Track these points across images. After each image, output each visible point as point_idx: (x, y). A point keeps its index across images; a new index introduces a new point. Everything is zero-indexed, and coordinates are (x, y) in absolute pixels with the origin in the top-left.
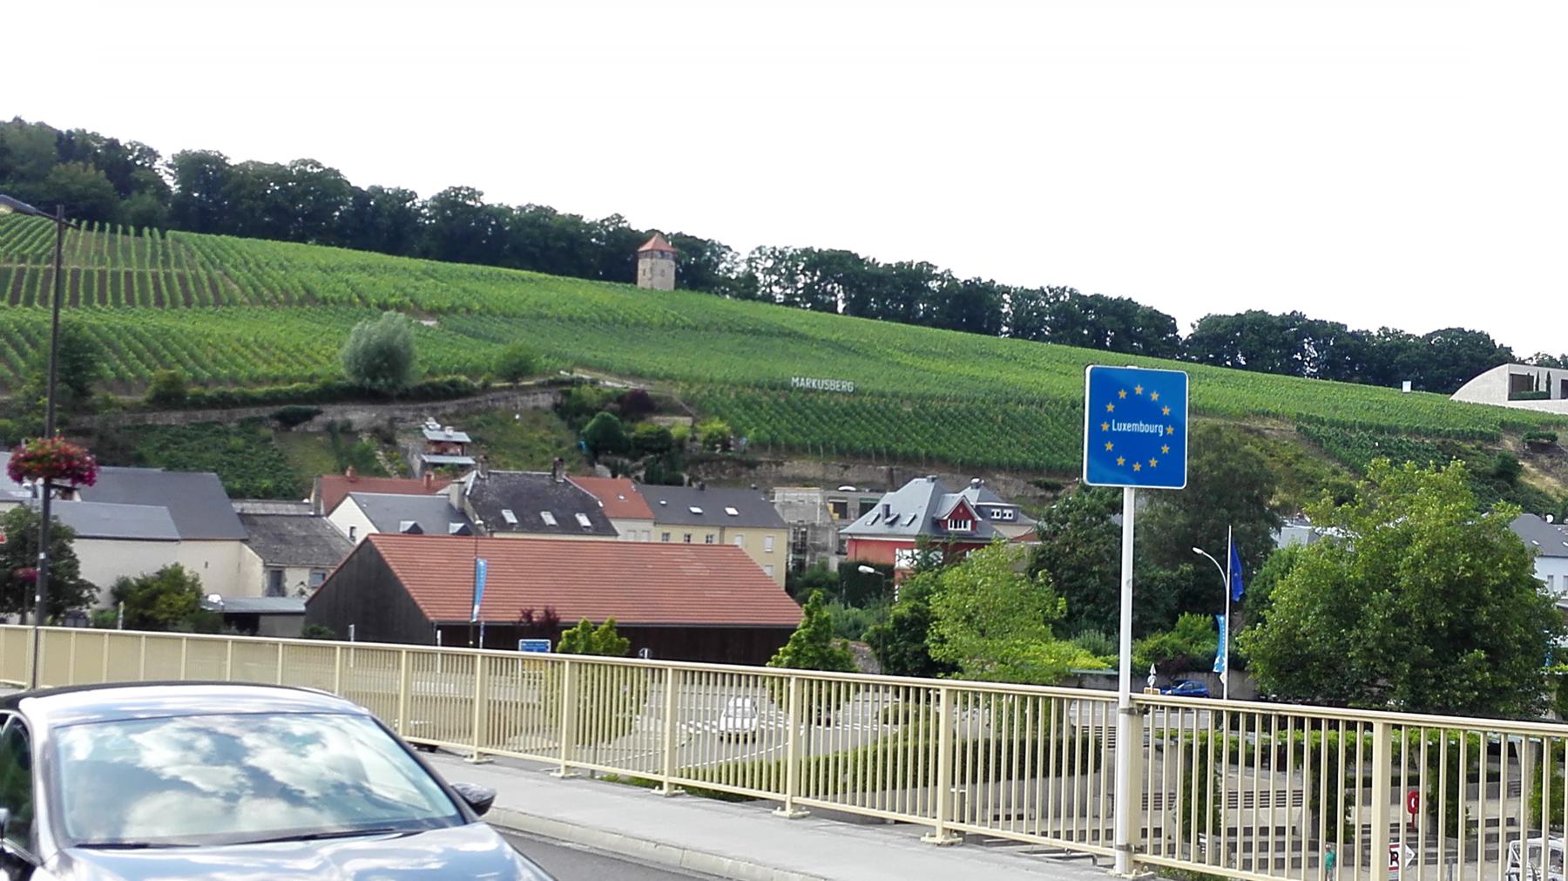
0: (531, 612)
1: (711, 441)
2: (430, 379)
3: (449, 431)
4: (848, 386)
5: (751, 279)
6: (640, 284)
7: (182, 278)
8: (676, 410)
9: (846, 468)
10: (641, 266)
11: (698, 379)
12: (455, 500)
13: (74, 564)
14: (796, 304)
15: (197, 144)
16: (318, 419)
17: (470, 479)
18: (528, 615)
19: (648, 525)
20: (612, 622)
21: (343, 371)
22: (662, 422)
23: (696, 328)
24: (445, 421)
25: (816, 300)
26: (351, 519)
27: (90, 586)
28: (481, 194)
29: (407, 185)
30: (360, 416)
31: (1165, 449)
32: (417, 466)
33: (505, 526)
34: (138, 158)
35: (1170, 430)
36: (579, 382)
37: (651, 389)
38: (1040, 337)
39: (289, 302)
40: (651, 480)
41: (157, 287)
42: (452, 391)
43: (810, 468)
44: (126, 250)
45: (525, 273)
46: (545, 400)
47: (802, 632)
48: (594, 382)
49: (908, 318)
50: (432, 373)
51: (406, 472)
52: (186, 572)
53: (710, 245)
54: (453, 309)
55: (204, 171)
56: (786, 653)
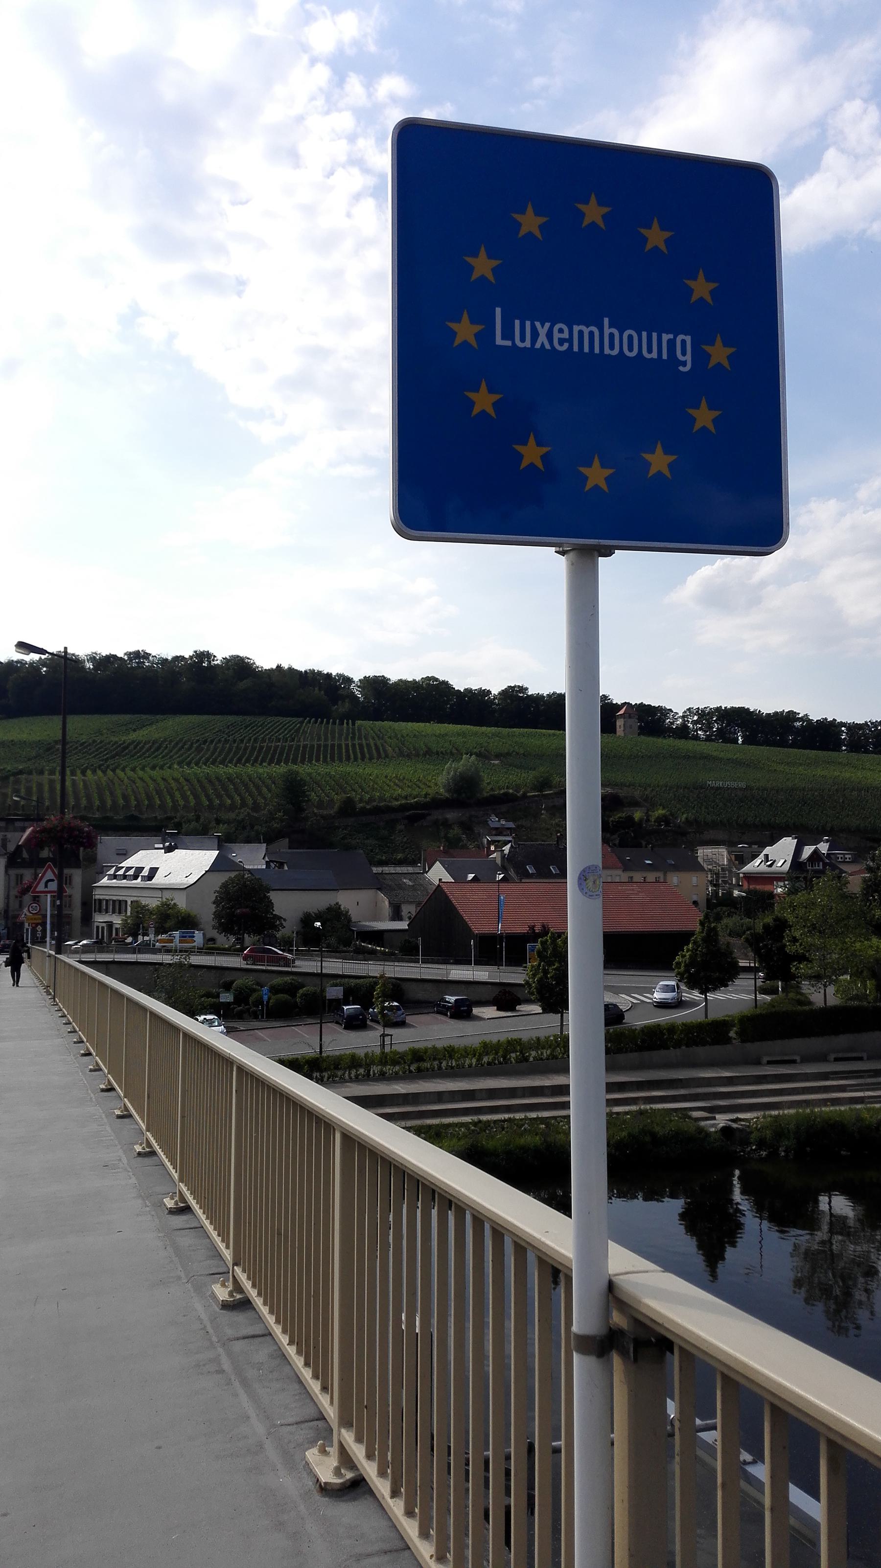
0: (534, 926)
1: (659, 820)
2: (491, 793)
3: (503, 822)
4: (742, 785)
5: (684, 726)
6: (618, 734)
7: (361, 746)
8: (636, 804)
9: (743, 833)
11: (649, 786)
12: (499, 861)
13: (270, 905)
14: (713, 740)
15: (371, 672)
16: (429, 818)
18: (532, 928)
19: (619, 872)
23: (650, 757)
24: (500, 816)
25: (724, 736)
26: (438, 874)
27: (280, 918)
28: (527, 689)
30: (451, 815)
31: (704, 417)
37: (622, 793)
38: (867, 752)
39: (417, 755)
41: (347, 751)
42: (506, 799)
43: (721, 835)
44: (333, 732)
47: (698, 937)
49: (783, 744)
50: (492, 789)
51: (480, 847)
52: (342, 907)
53: (659, 709)
54: (508, 754)
56: (688, 950)
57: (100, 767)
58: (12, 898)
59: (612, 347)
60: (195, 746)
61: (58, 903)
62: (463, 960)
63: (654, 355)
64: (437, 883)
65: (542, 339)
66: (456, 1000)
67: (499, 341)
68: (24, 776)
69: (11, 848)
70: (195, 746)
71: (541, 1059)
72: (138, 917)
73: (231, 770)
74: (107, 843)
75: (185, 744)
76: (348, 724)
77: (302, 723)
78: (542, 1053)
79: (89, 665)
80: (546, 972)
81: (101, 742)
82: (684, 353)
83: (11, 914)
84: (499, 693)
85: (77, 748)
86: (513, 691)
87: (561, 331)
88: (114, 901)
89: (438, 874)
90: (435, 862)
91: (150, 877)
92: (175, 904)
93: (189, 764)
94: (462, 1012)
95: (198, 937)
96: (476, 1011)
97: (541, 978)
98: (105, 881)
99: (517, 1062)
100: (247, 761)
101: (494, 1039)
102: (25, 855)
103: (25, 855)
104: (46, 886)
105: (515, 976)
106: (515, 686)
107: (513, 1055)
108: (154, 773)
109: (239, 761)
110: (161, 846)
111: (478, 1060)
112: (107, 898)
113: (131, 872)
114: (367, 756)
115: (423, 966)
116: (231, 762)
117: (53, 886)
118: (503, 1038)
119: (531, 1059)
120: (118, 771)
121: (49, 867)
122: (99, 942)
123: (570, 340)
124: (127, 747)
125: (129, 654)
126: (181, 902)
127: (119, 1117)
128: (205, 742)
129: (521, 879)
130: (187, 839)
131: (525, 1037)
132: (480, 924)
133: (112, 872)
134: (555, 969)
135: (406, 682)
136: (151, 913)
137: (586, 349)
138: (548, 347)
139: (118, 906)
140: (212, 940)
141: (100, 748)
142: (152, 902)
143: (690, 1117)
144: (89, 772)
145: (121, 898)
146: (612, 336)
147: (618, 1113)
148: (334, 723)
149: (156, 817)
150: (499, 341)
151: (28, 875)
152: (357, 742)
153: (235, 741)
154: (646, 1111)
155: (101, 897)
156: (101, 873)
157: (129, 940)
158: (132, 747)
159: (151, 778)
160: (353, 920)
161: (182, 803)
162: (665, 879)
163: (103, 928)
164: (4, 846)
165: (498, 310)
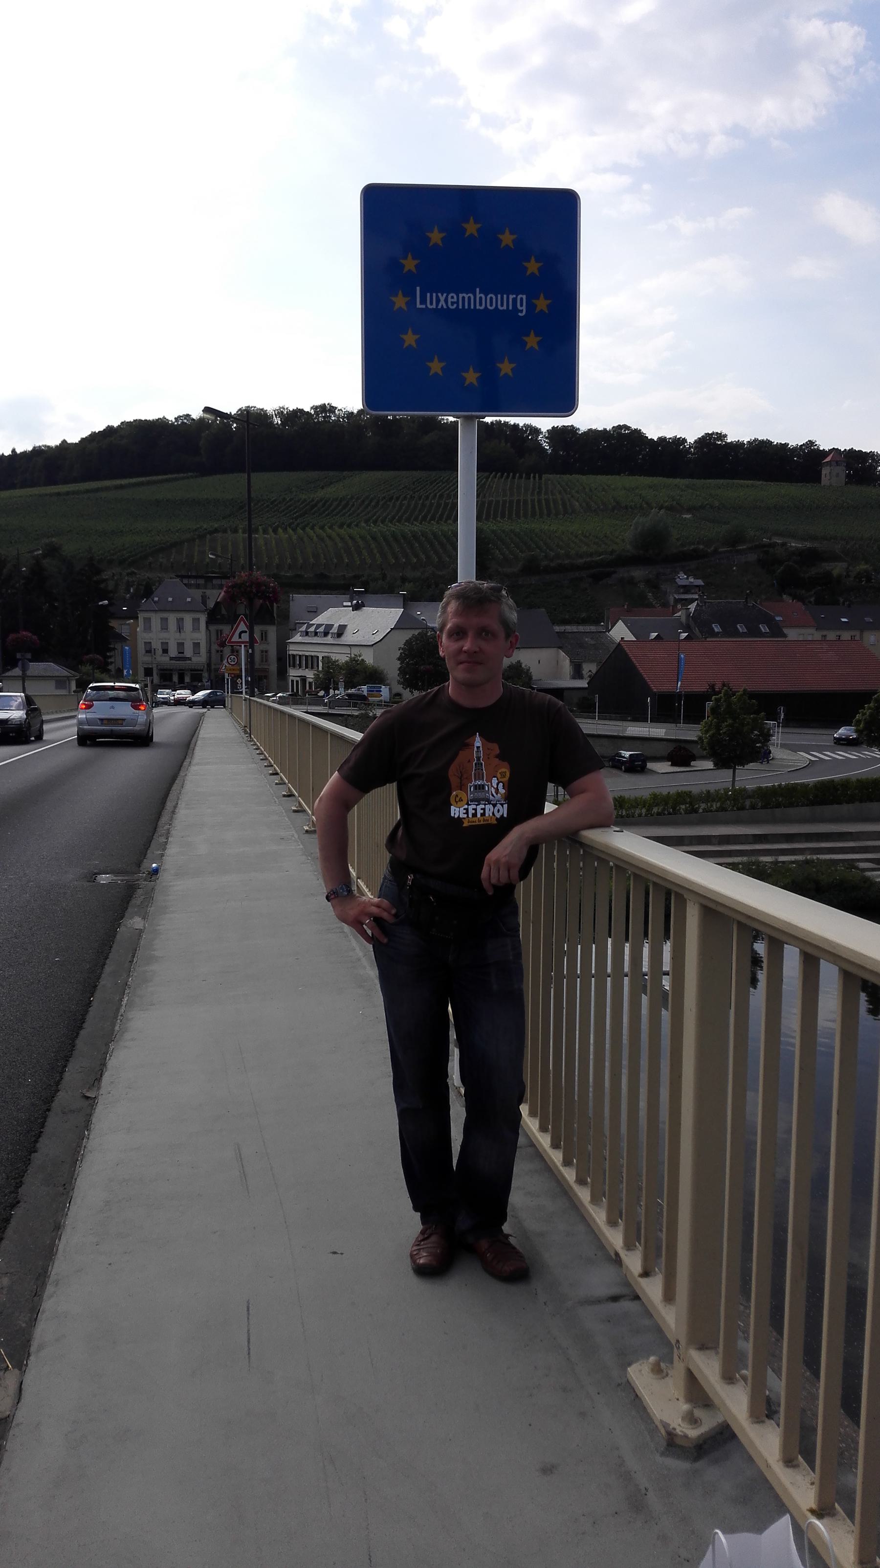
3: (691, 580)
6: (823, 483)
7: (547, 501)
8: (835, 558)
10: (824, 472)
12: (683, 619)
17: (692, 607)
18: (712, 687)
20: (745, 690)
21: (628, 547)
22: (827, 566)
26: (620, 632)
28: (725, 436)
29: (323, 403)
30: (638, 573)
32: (672, 602)
33: (714, 634)
34: (529, 435)
35: (542, 304)
36: (773, 545)
40: (819, 602)
41: (533, 507)
42: (695, 555)
45: (750, 482)
46: (752, 557)
48: (784, 544)
51: (665, 605)
52: (523, 666)
55: (282, 412)
56: (869, 708)
57: (290, 525)
58: (213, 651)
59: (481, 304)
60: (381, 503)
61: (250, 651)
62: (639, 717)
63: (505, 307)
64: (618, 640)
65: (442, 302)
66: (630, 755)
67: (419, 306)
68: (220, 535)
69: (211, 604)
70: (381, 503)
71: (711, 811)
72: (328, 672)
73: (417, 527)
74: (299, 601)
75: (371, 501)
76: (534, 477)
77: (487, 478)
78: (712, 806)
79: (277, 421)
80: (718, 727)
81: (291, 500)
82: (522, 305)
83: (213, 667)
84: (696, 442)
85: (268, 506)
86: (710, 439)
87: (452, 297)
88: (307, 657)
89: (620, 632)
90: (617, 621)
91: (340, 633)
92: (363, 660)
93: (375, 522)
94: (636, 766)
95: (385, 691)
96: (650, 765)
97: (713, 735)
98: (298, 638)
99: (686, 813)
100: (433, 518)
101: (665, 792)
102: (224, 612)
103: (224, 612)
104: (240, 637)
105: (689, 733)
106: (713, 433)
107: (683, 807)
108: (342, 531)
109: (424, 518)
110: (349, 604)
111: (648, 810)
112: (301, 653)
113: (321, 629)
114: (538, 513)
115: (599, 722)
116: (416, 519)
117: (246, 637)
118: (673, 791)
119: (701, 811)
120: (308, 529)
121: (242, 619)
122: (294, 695)
123: (457, 303)
124: (316, 505)
125: (315, 408)
126: (368, 658)
127: (295, 811)
128: (391, 499)
129: (706, 638)
130: (371, 597)
131: (695, 790)
132: (659, 683)
133: (304, 628)
134: (727, 726)
135: (595, 432)
136: (341, 668)
137: (466, 307)
138: (445, 307)
139: (310, 661)
140: (399, 695)
141: (290, 506)
142: (341, 657)
143: (857, 868)
144: (280, 530)
145: (313, 654)
146: (481, 298)
147: (783, 862)
148: (520, 477)
149: (344, 576)
150: (419, 306)
151: (226, 629)
152: (543, 497)
153: (420, 498)
154: (813, 861)
155: (295, 653)
156: (295, 630)
157: (322, 693)
158: (320, 505)
159: (338, 535)
160: (534, 678)
161: (369, 561)
162: (861, 638)
163: (297, 682)
164: (204, 603)
165: (418, 288)
